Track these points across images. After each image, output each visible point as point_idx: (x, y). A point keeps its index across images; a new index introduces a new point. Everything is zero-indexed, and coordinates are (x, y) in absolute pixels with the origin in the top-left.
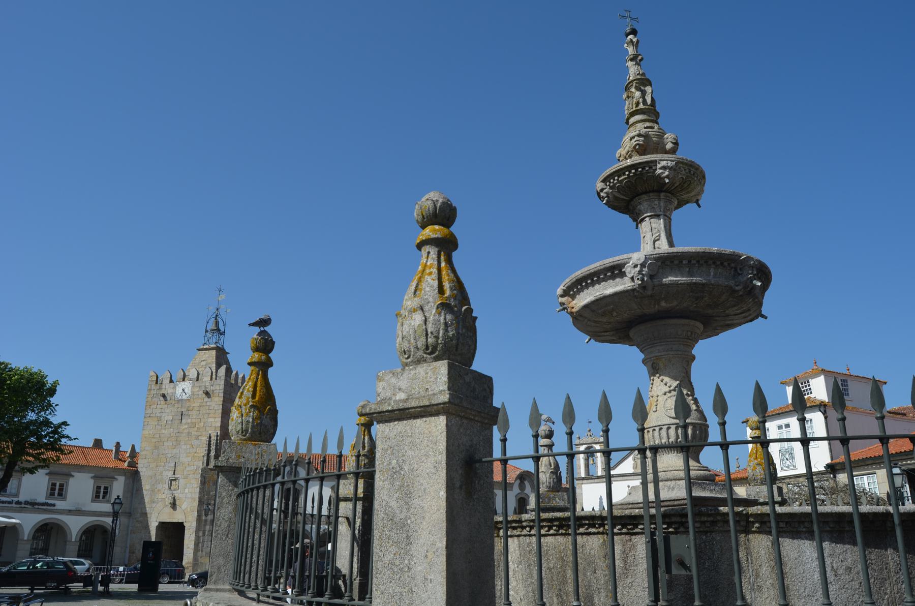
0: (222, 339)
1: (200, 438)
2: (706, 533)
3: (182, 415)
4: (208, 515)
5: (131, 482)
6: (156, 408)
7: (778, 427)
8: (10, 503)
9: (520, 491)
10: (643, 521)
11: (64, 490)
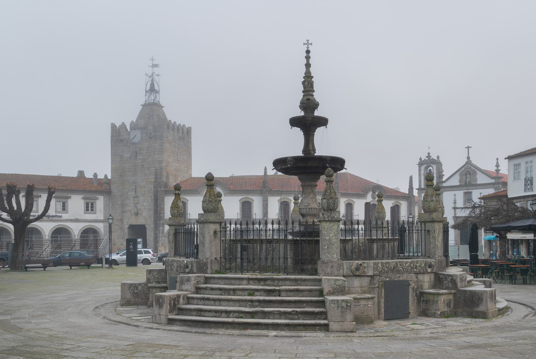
0: (158, 97)
2: (276, 243)
3: (136, 153)
4: (160, 220)
5: (108, 199)
6: (118, 149)
7: (515, 165)
9: (372, 200)
11: (66, 206)
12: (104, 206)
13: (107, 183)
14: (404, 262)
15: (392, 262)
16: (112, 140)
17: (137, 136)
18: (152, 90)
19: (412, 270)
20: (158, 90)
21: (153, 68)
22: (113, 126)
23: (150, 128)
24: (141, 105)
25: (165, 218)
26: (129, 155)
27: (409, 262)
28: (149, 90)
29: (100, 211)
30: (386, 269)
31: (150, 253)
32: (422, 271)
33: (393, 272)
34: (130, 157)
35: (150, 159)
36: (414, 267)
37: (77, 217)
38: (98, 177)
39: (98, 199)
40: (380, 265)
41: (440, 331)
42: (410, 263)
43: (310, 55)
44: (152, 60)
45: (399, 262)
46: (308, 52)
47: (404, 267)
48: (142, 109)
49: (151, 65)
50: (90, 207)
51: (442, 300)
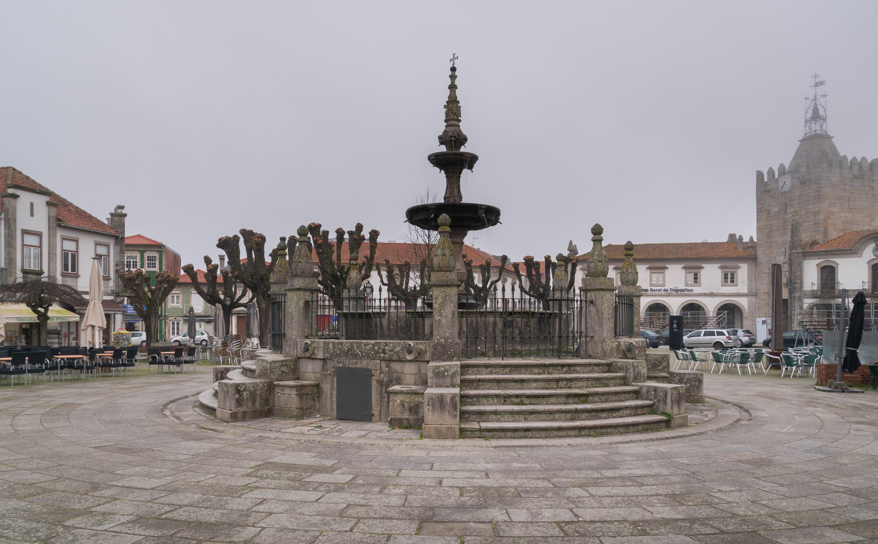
1: (803, 224)
8: (659, 290)
10: (358, 318)
12: (748, 276)
13: (752, 247)
14: (362, 343)
15: (346, 343)
16: (757, 192)
17: (787, 183)
18: (816, 116)
19: (376, 355)
20: (824, 116)
21: (817, 88)
22: (760, 175)
23: (803, 169)
24: (799, 141)
25: (805, 289)
26: (777, 209)
27: (371, 344)
28: (810, 118)
29: (743, 282)
30: (338, 352)
31: (724, 335)
32: (395, 357)
33: (347, 356)
34: (778, 212)
35: (803, 211)
36: (381, 351)
37: (712, 291)
38: (744, 241)
39: (740, 267)
40: (331, 346)
41: (272, 436)
42: (374, 345)
43: (457, 73)
44: (816, 77)
45: (356, 343)
46: (453, 69)
47: (363, 350)
48: (800, 146)
49: (814, 84)
50: (729, 278)
51: (398, 401)
